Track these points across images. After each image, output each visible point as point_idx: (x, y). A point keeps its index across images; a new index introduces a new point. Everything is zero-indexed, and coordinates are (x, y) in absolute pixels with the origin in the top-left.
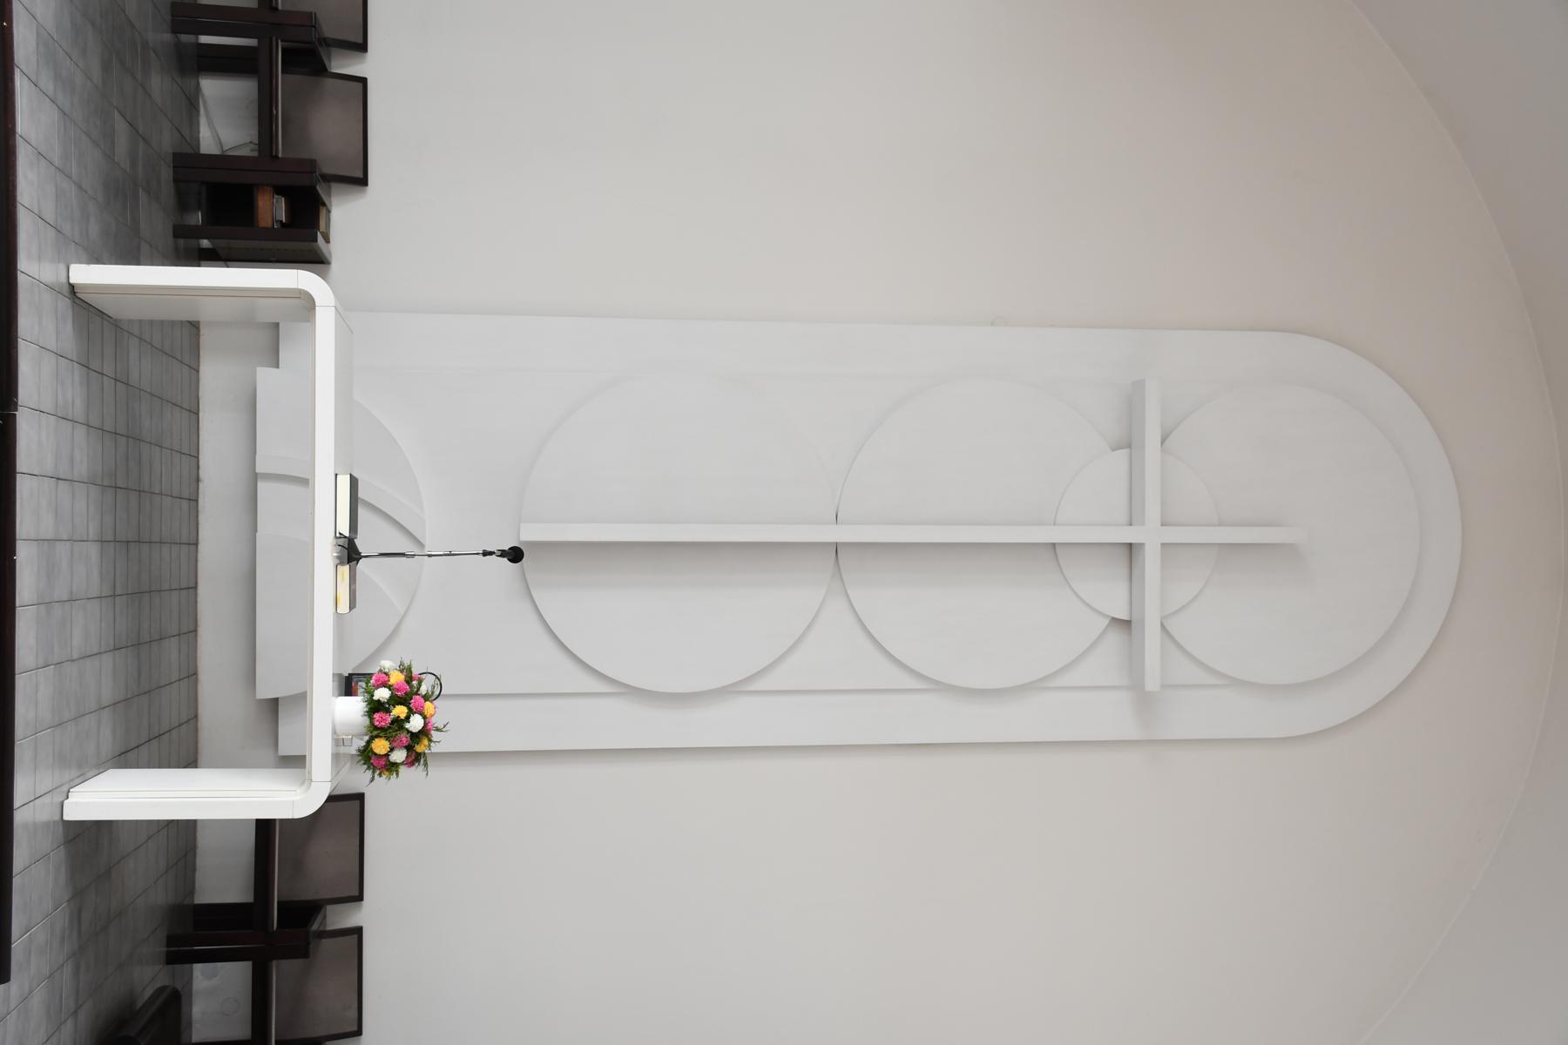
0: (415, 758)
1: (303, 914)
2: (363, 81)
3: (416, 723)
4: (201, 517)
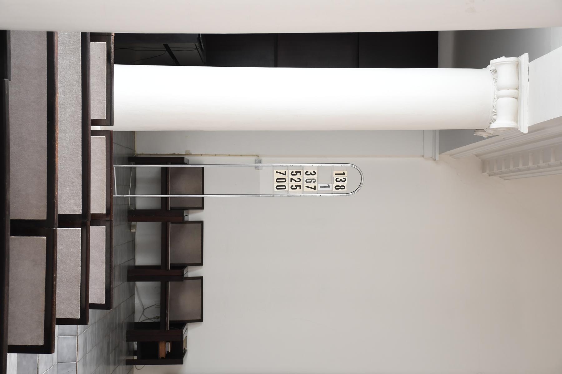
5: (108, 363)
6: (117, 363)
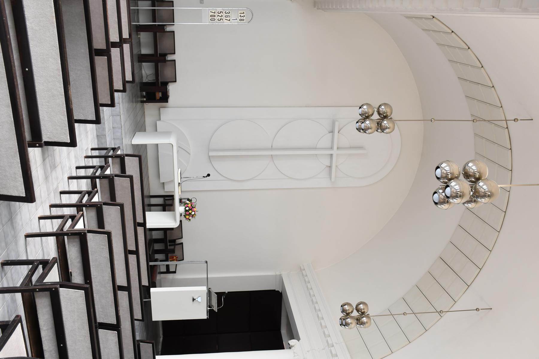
3: (193, 213)
5: (133, 102)
6: (137, 102)
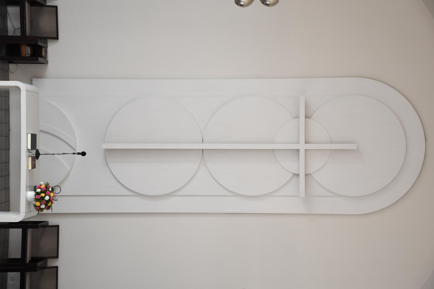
0: (48, 208)
1: (44, 259)
2: (56, 7)
3: (47, 198)
4: (11, 141)
